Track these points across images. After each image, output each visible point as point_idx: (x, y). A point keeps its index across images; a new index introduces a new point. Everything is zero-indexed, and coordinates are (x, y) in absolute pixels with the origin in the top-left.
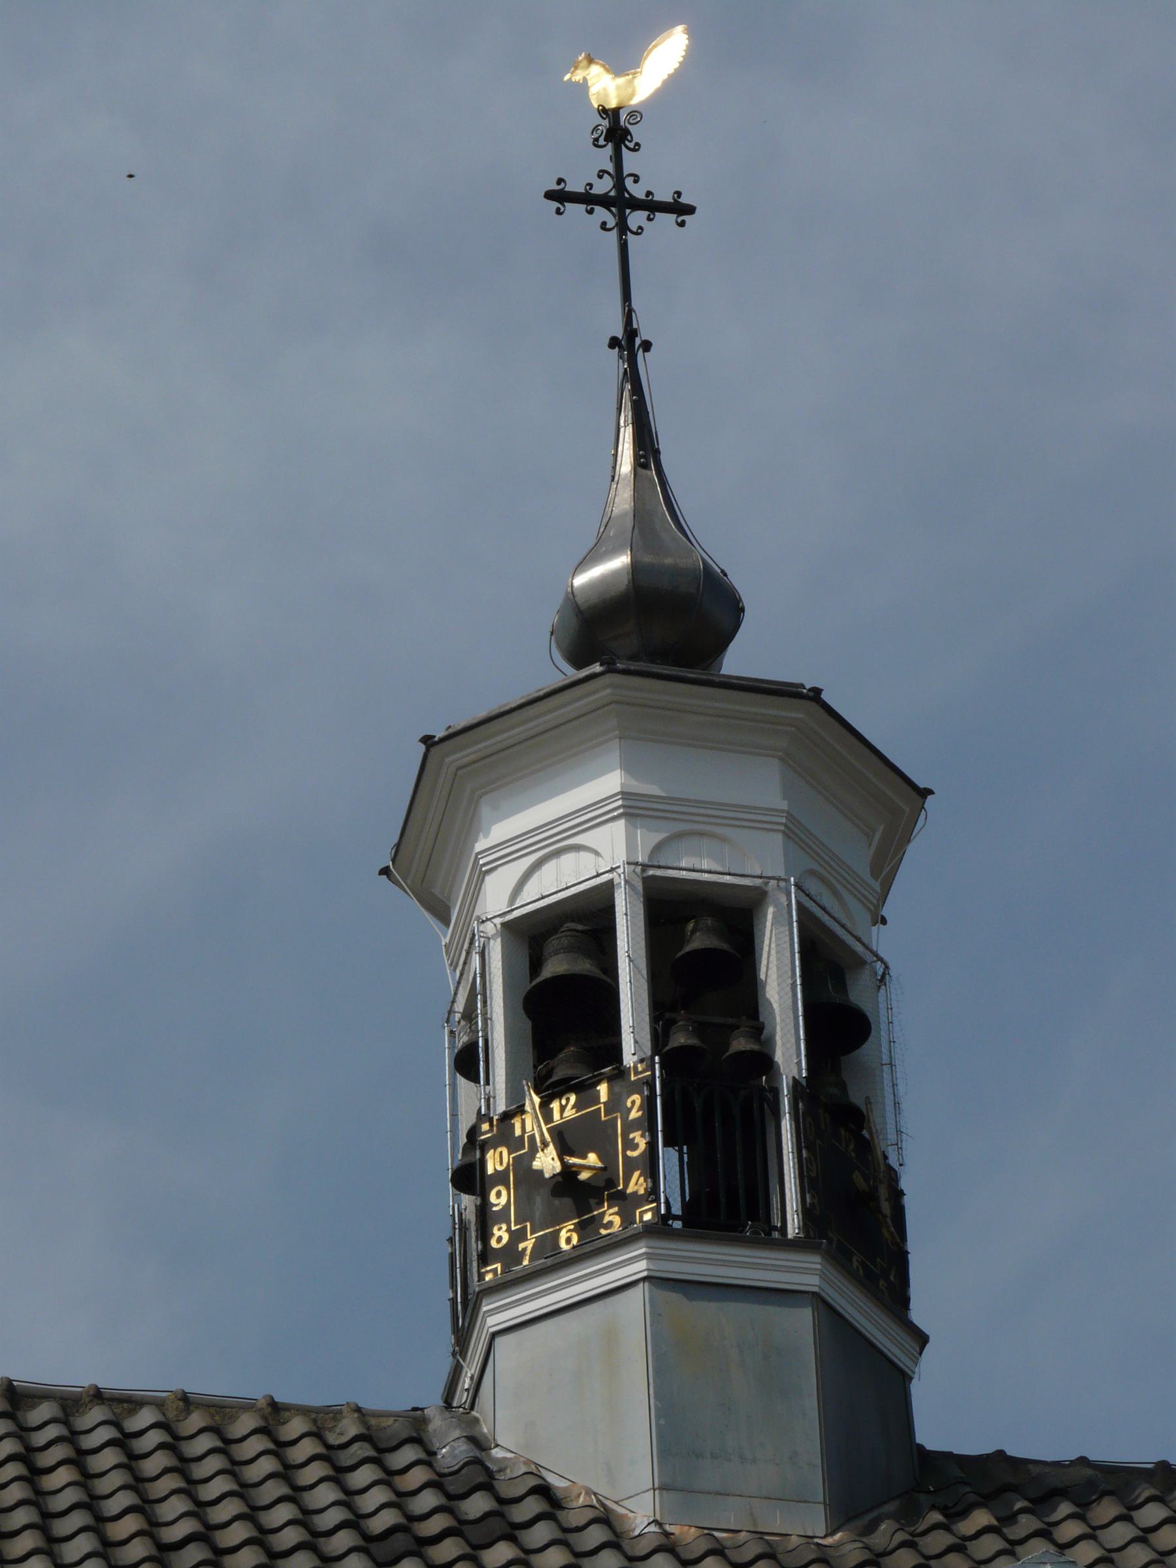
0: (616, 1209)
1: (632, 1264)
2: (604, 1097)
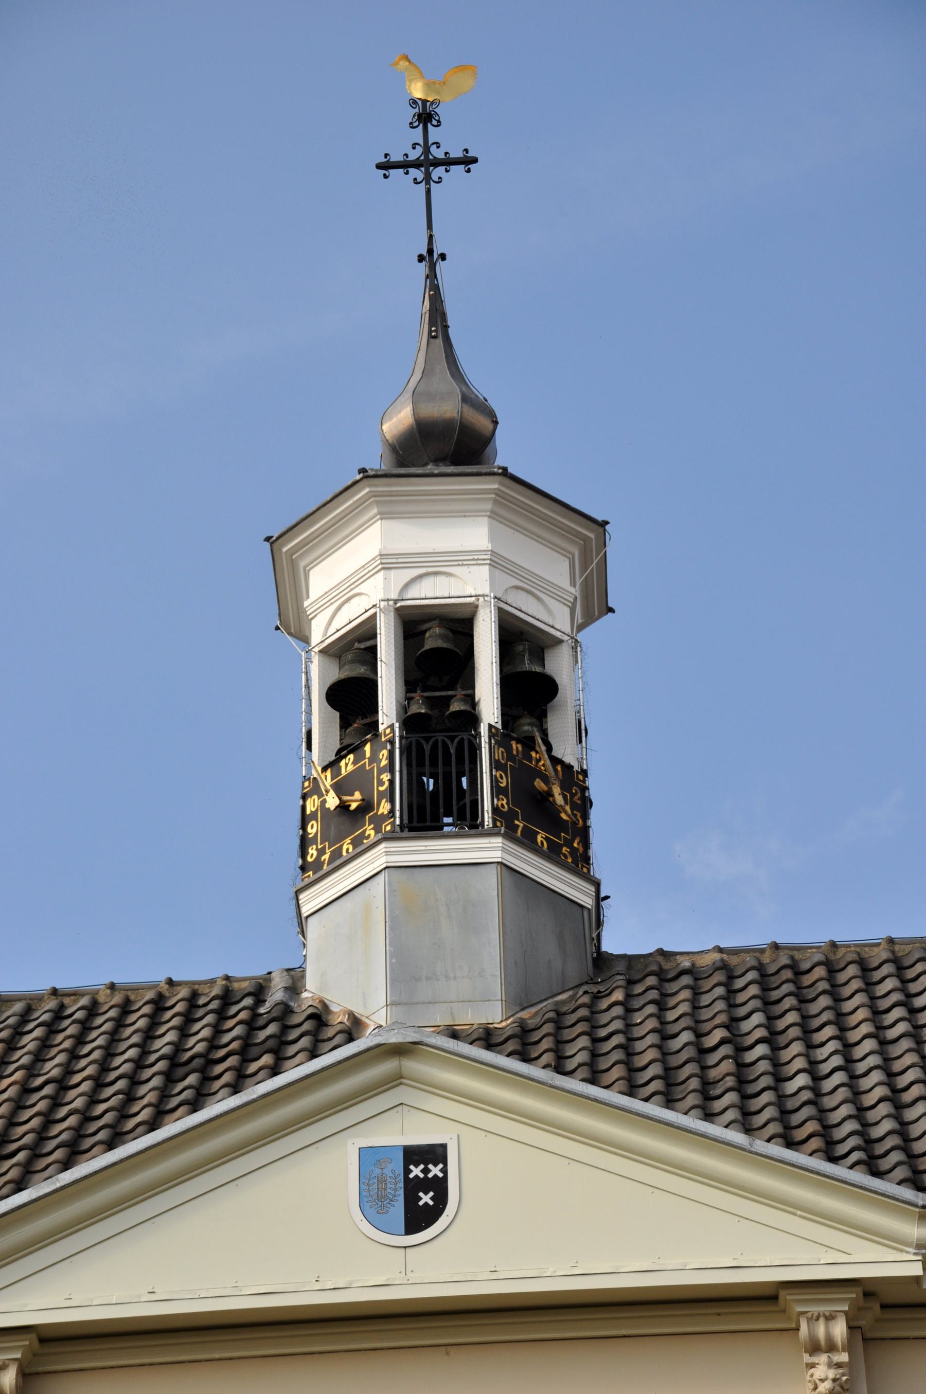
0: (372, 826)
2: (368, 755)
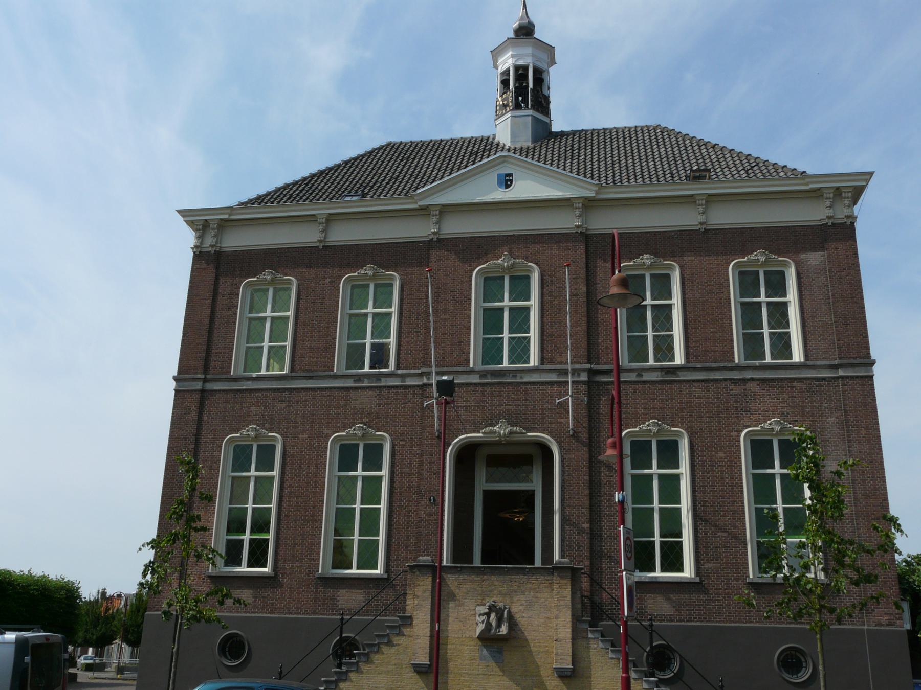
1: (509, 115)
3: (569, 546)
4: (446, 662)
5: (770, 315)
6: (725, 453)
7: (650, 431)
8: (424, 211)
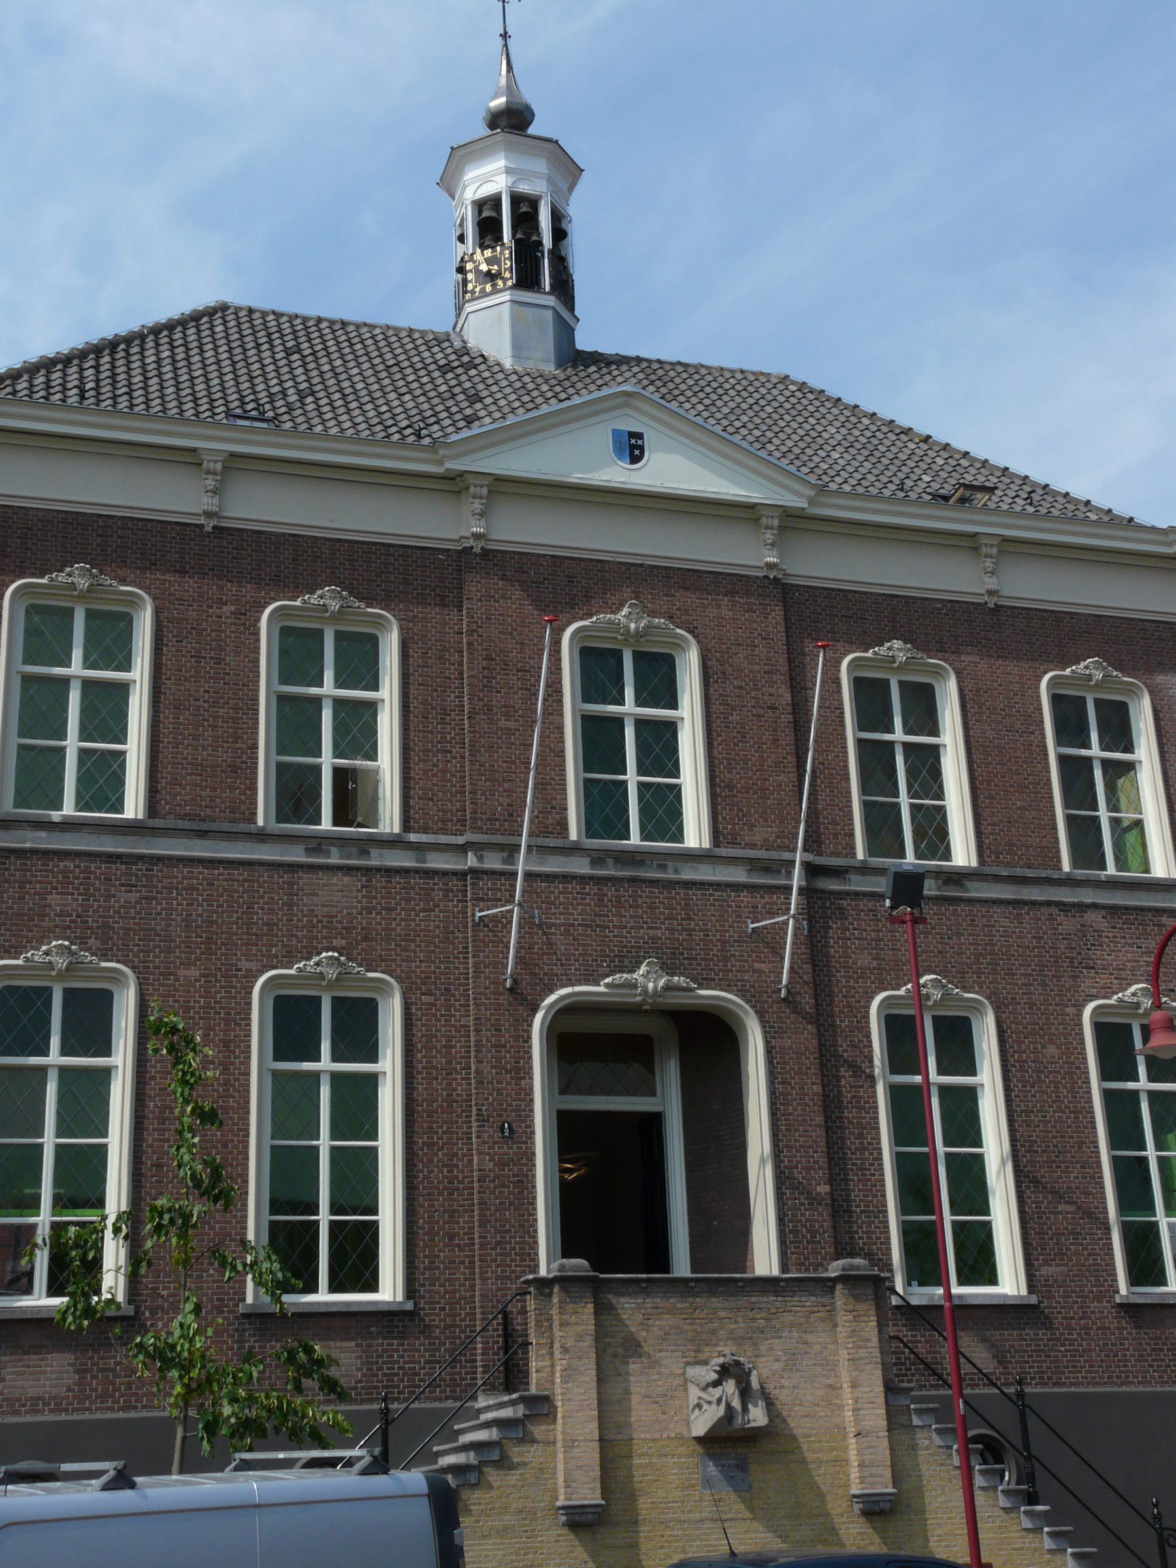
3: (794, 1232)
4: (632, 1497)
5: (338, 729)
6: (1058, 1047)
7: (321, 976)
8: (453, 485)
